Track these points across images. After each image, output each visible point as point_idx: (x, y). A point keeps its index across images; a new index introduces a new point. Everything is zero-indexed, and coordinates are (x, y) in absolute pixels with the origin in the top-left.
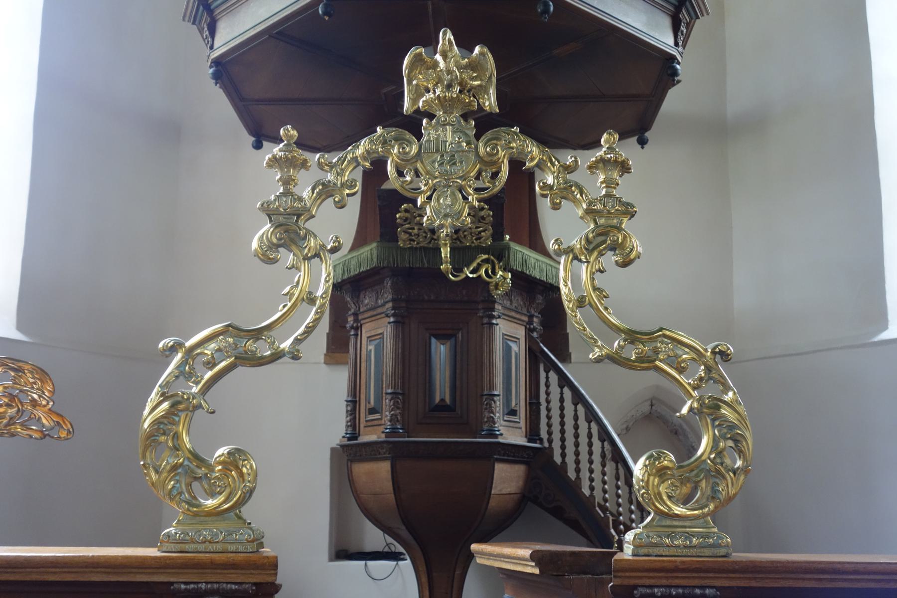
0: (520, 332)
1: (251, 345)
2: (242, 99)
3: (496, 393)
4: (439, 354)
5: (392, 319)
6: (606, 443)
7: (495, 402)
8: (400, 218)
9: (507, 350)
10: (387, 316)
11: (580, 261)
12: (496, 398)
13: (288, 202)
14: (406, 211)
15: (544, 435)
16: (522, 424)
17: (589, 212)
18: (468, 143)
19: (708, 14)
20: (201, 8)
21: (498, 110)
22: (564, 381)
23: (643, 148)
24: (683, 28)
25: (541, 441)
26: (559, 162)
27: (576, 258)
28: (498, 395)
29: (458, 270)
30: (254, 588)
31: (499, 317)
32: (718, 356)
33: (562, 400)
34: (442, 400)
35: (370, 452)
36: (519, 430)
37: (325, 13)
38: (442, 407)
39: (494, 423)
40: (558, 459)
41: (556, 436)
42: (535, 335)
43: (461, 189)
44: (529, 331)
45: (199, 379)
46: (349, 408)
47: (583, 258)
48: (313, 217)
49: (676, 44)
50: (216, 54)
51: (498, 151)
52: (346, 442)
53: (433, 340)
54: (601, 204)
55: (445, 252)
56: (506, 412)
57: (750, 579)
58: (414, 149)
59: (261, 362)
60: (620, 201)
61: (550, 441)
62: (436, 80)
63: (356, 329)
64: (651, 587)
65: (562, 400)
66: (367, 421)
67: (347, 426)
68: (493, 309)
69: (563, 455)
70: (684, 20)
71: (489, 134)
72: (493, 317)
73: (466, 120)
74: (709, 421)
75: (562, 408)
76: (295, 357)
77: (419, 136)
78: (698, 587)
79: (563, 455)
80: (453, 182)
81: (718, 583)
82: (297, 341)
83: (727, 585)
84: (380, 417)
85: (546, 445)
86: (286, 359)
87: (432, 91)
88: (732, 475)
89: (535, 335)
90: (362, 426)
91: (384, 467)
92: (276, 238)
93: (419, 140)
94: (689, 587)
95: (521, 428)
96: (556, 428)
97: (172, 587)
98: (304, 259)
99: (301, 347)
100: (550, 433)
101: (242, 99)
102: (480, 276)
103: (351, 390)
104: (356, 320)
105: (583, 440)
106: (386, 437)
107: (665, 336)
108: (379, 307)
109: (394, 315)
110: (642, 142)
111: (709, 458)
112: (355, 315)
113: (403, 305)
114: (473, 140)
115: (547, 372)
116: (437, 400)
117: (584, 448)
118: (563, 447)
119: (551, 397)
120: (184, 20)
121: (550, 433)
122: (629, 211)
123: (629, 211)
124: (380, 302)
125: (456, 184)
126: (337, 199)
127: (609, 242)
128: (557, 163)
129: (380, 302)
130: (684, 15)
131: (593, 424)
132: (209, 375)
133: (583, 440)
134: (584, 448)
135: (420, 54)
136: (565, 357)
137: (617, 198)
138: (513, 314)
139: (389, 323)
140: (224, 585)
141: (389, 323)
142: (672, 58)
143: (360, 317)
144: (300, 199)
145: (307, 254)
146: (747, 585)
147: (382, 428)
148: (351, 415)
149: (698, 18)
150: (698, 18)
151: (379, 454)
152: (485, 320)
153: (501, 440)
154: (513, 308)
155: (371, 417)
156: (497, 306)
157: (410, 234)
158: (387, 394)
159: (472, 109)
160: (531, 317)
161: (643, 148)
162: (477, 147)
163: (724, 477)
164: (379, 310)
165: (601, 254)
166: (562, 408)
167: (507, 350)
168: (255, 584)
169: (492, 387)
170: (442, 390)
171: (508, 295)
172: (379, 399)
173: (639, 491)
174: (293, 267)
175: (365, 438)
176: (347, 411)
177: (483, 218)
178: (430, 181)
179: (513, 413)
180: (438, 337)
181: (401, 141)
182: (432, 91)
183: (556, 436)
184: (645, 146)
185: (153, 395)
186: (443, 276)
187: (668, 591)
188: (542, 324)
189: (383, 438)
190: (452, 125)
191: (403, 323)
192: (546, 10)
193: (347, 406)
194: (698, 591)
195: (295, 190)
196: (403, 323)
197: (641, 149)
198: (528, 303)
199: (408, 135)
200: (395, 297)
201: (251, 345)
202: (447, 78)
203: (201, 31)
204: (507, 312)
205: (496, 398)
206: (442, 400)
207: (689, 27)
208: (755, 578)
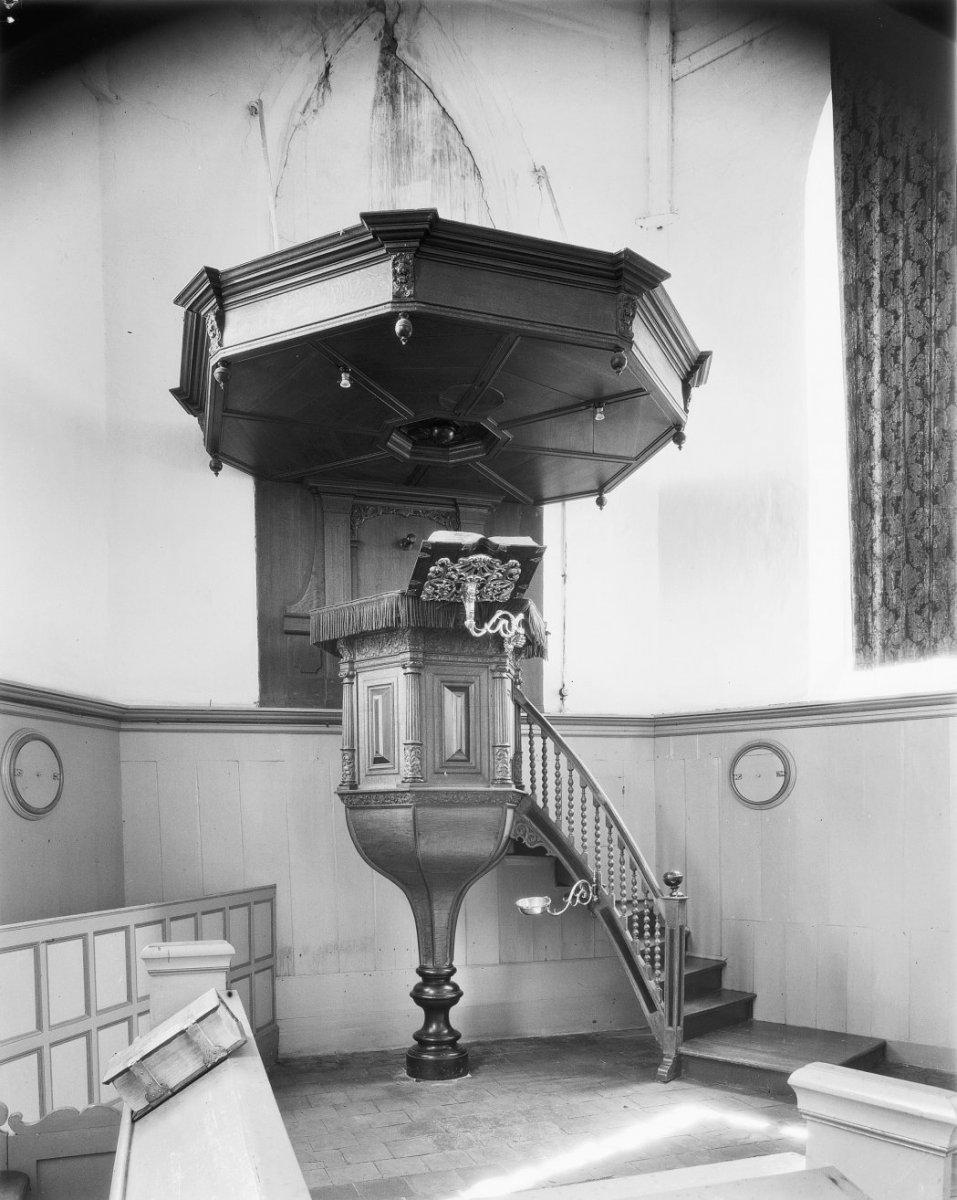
3: (507, 744)
4: (391, 707)
5: (409, 670)
6: (587, 789)
12: (508, 749)
14: (442, 565)
15: (526, 780)
23: (217, 474)
29: (480, 623)
33: (544, 750)
37: (403, 333)
41: (539, 783)
52: (346, 789)
53: (448, 693)
55: (470, 607)
61: (533, 788)
63: (352, 677)
65: (544, 750)
69: (545, 800)
75: (544, 758)
79: (545, 800)
84: (464, 758)
90: (362, 775)
96: (539, 776)
100: (533, 780)
104: (352, 669)
109: (411, 667)
110: (600, 502)
112: (351, 662)
113: (420, 656)
116: (455, 750)
118: (545, 793)
120: (176, 302)
121: (533, 780)
131: (575, 772)
143: (355, 666)
152: (497, 674)
157: (436, 588)
161: (217, 474)
166: (544, 758)
169: (505, 738)
170: (454, 742)
175: (364, 787)
177: (511, 575)
180: (453, 689)
183: (539, 783)
186: (466, 631)
205: (508, 749)
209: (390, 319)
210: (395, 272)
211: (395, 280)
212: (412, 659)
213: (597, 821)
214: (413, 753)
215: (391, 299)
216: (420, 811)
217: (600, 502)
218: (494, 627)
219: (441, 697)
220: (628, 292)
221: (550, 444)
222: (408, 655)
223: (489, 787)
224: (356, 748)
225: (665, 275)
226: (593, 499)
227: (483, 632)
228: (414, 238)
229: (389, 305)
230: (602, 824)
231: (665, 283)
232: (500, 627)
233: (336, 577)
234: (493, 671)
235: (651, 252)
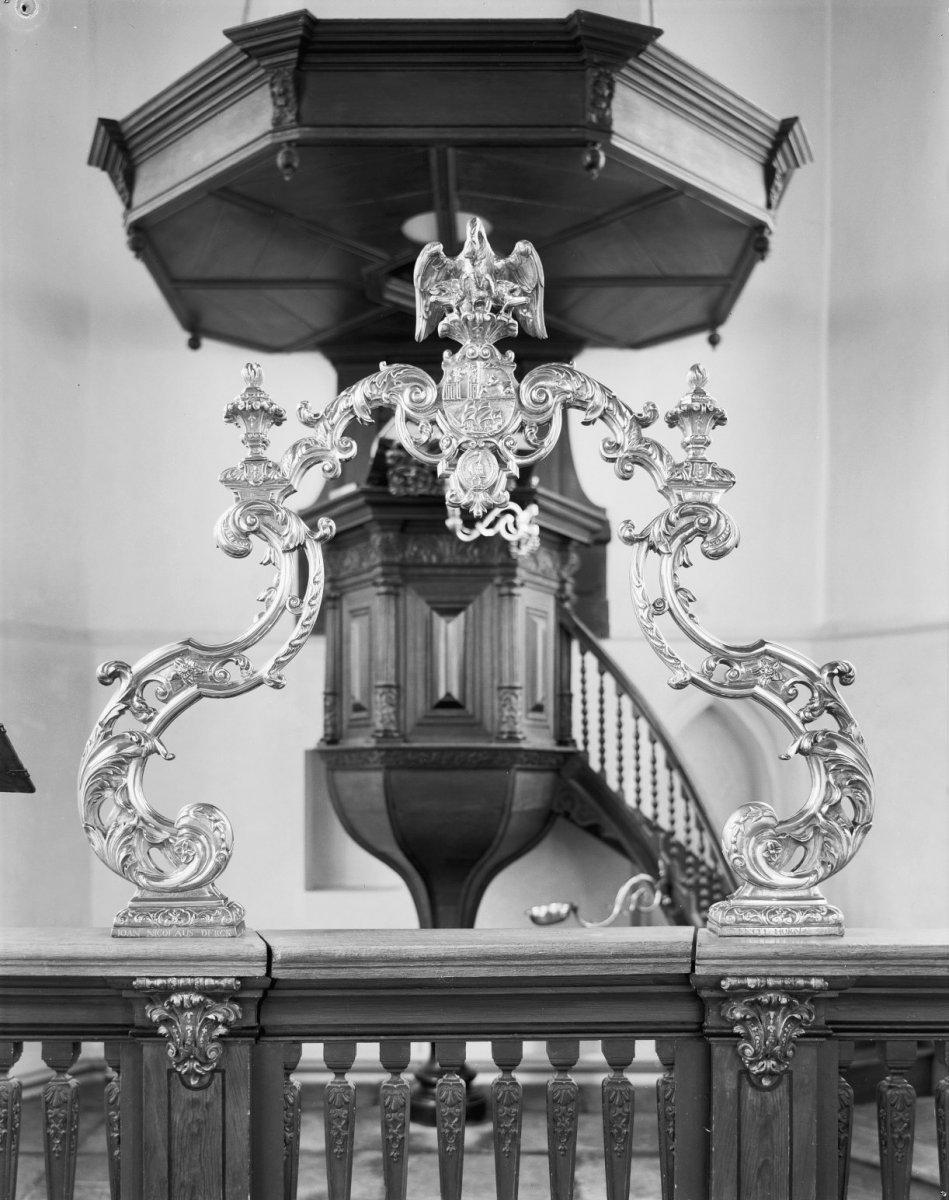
0: (549, 604)
1: (213, 670)
2: (175, 281)
5: (382, 589)
7: (516, 697)
8: (392, 457)
9: (531, 628)
10: (375, 584)
11: (659, 551)
13: (258, 472)
15: (577, 733)
16: (551, 722)
17: (674, 483)
18: (507, 385)
19: (812, 160)
20: (114, 148)
21: (546, 336)
22: (606, 665)
24: (778, 183)
25: (574, 742)
26: (631, 413)
27: (652, 547)
28: (520, 688)
30: (239, 983)
31: (522, 585)
32: (836, 679)
34: (448, 695)
35: (356, 760)
36: (547, 731)
37: (288, 165)
38: (449, 703)
39: (515, 724)
40: (595, 765)
41: (594, 737)
42: (567, 605)
43: (495, 451)
44: (560, 600)
45: (152, 714)
46: (328, 704)
47: (662, 548)
48: (295, 491)
49: (769, 205)
50: (135, 216)
51: (547, 397)
52: (325, 747)
54: (688, 472)
56: (530, 707)
57: (868, 966)
58: (430, 394)
59: (232, 692)
60: (713, 468)
62: (462, 293)
64: (743, 977)
66: (352, 720)
67: (326, 726)
68: (514, 575)
70: (780, 171)
71: (536, 372)
72: (513, 585)
73: (503, 352)
74: (821, 762)
76: (277, 686)
77: (438, 376)
78: (801, 977)
79: (602, 761)
80: (486, 442)
81: (827, 972)
82: (279, 664)
83: (838, 974)
85: (580, 747)
86: (264, 689)
87: (455, 310)
88: (848, 832)
89: (567, 605)
90: (345, 726)
91: (376, 779)
92: (246, 523)
93: (438, 381)
94: (791, 977)
95: (548, 727)
97: (134, 983)
98: (284, 552)
99: (283, 672)
101: (175, 281)
102: (498, 535)
103: (100, 155)
105: (628, 742)
106: (378, 742)
107: (766, 653)
108: (364, 572)
109: (384, 584)
110: (714, 341)
111: (820, 811)
113: (396, 569)
114: (514, 381)
115: (583, 653)
117: (628, 752)
119: (588, 686)
122: (724, 479)
123: (724, 479)
124: (365, 565)
125: (490, 445)
126: (327, 468)
127: (697, 526)
128: (628, 414)
129: (365, 565)
130: (780, 163)
132: (164, 710)
133: (628, 742)
134: (628, 752)
135: (437, 254)
136: (603, 630)
137: (710, 464)
138: (539, 580)
139: (379, 594)
140: (201, 980)
141: (379, 594)
142: (760, 227)
144: (276, 467)
145: (288, 546)
146: (864, 974)
147: (371, 730)
148: (330, 711)
149: (797, 165)
150: (797, 165)
151: (369, 762)
152: (505, 590)
153: (524, 745)
154: (539, 571)
155: (356, 715)
156: (520, 572)
157: (405, 478)
158: (378, 687)
159: (510, 334)
160: (563, 582)
162: (518, 390)
163: (839, 837)
164: (365, 576)
165: (686, 541)
167: (531, 628)
168: (238, 978)
169: (513, 675)
171: (533, 555)
172: (369, 689)
173: (729, 855)
174: (269, 562)
176: (326, 707)
178: (454, 441)
179: (539, 708)
181: (414, 384)
182: (455, 310)
183: (594, 737)
184: (722, 331)
185: (92, 737)
187: (763, 981)
188: (577, 591)
189: (372, 743)
190: (484, 360)
191: (397, 595)
192: (594, 164)
193: (325, 700)
194: (801, 982)
195: (266, 454)
196: (397, 595)
197: (708, 347)
198: (558, 565)
199: (419, 373)
200: (385, 559)
201: (213, 670)
202: (476, 294)
203: (114, 179)
204: (532, 578)
205: (518, 692)
206: (448, 695)
207: (785, 178)
208: (873, 966)
209: (274, 149)
210: (273, 95)
211: (275, 104)
212: (384, 574)
213: (672, 789)
214: (384, 697)
215: (270, 128)
216: (394, 775)
217: (714, 341)
218: (491, 526)
219: (431, 621)
220: (597, 65)
221: (390, 287)
222: (379, 570)
223: (491, 742)
224: (402, 683)
225: (658, 32)
226: (702, 338)
227: (475, 535)
228: (290, 48)
229: (269, 135)
230: (677, 793)
231: (661, 41)
232: (500, 527)
233: (708, 427)
234: (499, 586)
235: (222, 34)
